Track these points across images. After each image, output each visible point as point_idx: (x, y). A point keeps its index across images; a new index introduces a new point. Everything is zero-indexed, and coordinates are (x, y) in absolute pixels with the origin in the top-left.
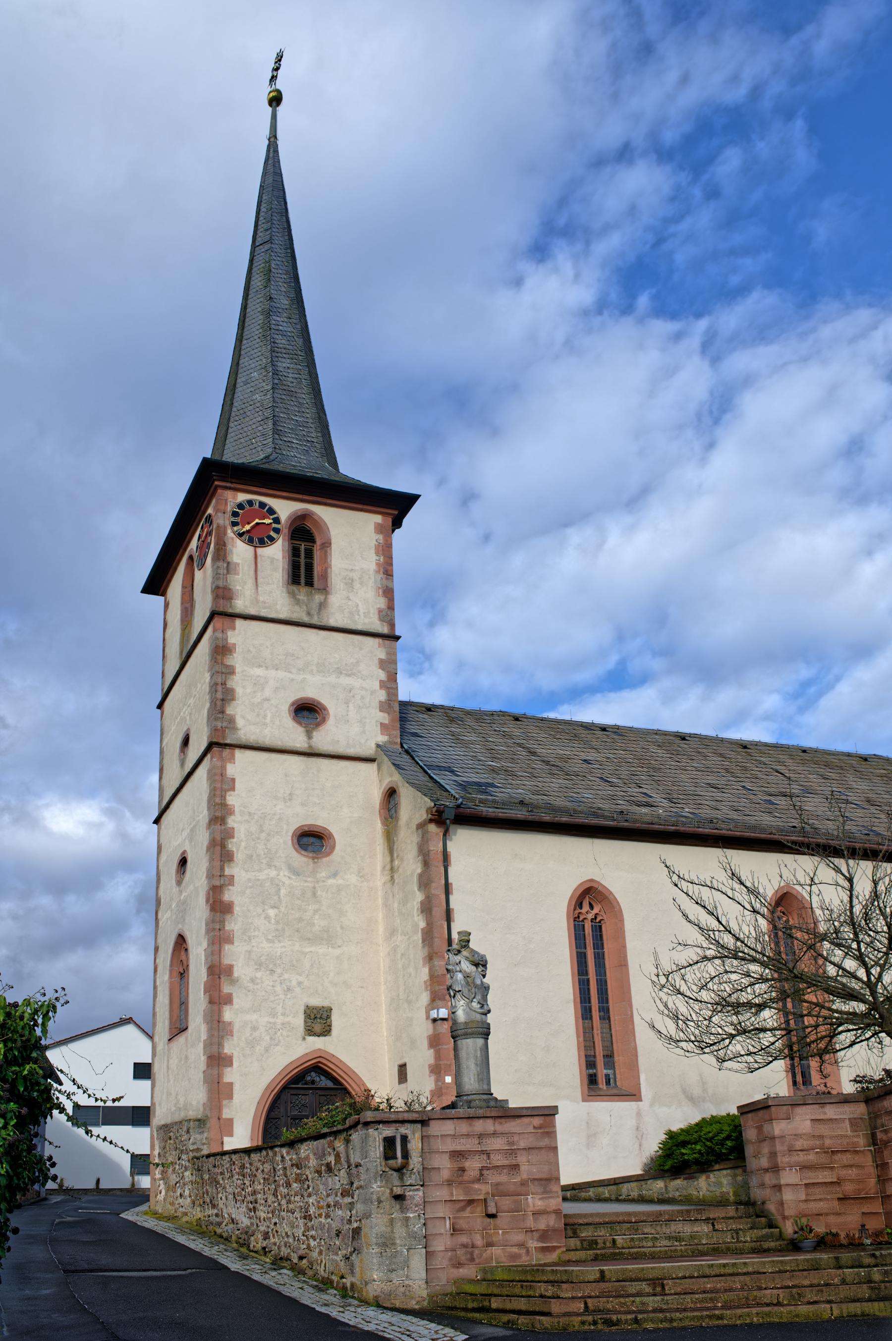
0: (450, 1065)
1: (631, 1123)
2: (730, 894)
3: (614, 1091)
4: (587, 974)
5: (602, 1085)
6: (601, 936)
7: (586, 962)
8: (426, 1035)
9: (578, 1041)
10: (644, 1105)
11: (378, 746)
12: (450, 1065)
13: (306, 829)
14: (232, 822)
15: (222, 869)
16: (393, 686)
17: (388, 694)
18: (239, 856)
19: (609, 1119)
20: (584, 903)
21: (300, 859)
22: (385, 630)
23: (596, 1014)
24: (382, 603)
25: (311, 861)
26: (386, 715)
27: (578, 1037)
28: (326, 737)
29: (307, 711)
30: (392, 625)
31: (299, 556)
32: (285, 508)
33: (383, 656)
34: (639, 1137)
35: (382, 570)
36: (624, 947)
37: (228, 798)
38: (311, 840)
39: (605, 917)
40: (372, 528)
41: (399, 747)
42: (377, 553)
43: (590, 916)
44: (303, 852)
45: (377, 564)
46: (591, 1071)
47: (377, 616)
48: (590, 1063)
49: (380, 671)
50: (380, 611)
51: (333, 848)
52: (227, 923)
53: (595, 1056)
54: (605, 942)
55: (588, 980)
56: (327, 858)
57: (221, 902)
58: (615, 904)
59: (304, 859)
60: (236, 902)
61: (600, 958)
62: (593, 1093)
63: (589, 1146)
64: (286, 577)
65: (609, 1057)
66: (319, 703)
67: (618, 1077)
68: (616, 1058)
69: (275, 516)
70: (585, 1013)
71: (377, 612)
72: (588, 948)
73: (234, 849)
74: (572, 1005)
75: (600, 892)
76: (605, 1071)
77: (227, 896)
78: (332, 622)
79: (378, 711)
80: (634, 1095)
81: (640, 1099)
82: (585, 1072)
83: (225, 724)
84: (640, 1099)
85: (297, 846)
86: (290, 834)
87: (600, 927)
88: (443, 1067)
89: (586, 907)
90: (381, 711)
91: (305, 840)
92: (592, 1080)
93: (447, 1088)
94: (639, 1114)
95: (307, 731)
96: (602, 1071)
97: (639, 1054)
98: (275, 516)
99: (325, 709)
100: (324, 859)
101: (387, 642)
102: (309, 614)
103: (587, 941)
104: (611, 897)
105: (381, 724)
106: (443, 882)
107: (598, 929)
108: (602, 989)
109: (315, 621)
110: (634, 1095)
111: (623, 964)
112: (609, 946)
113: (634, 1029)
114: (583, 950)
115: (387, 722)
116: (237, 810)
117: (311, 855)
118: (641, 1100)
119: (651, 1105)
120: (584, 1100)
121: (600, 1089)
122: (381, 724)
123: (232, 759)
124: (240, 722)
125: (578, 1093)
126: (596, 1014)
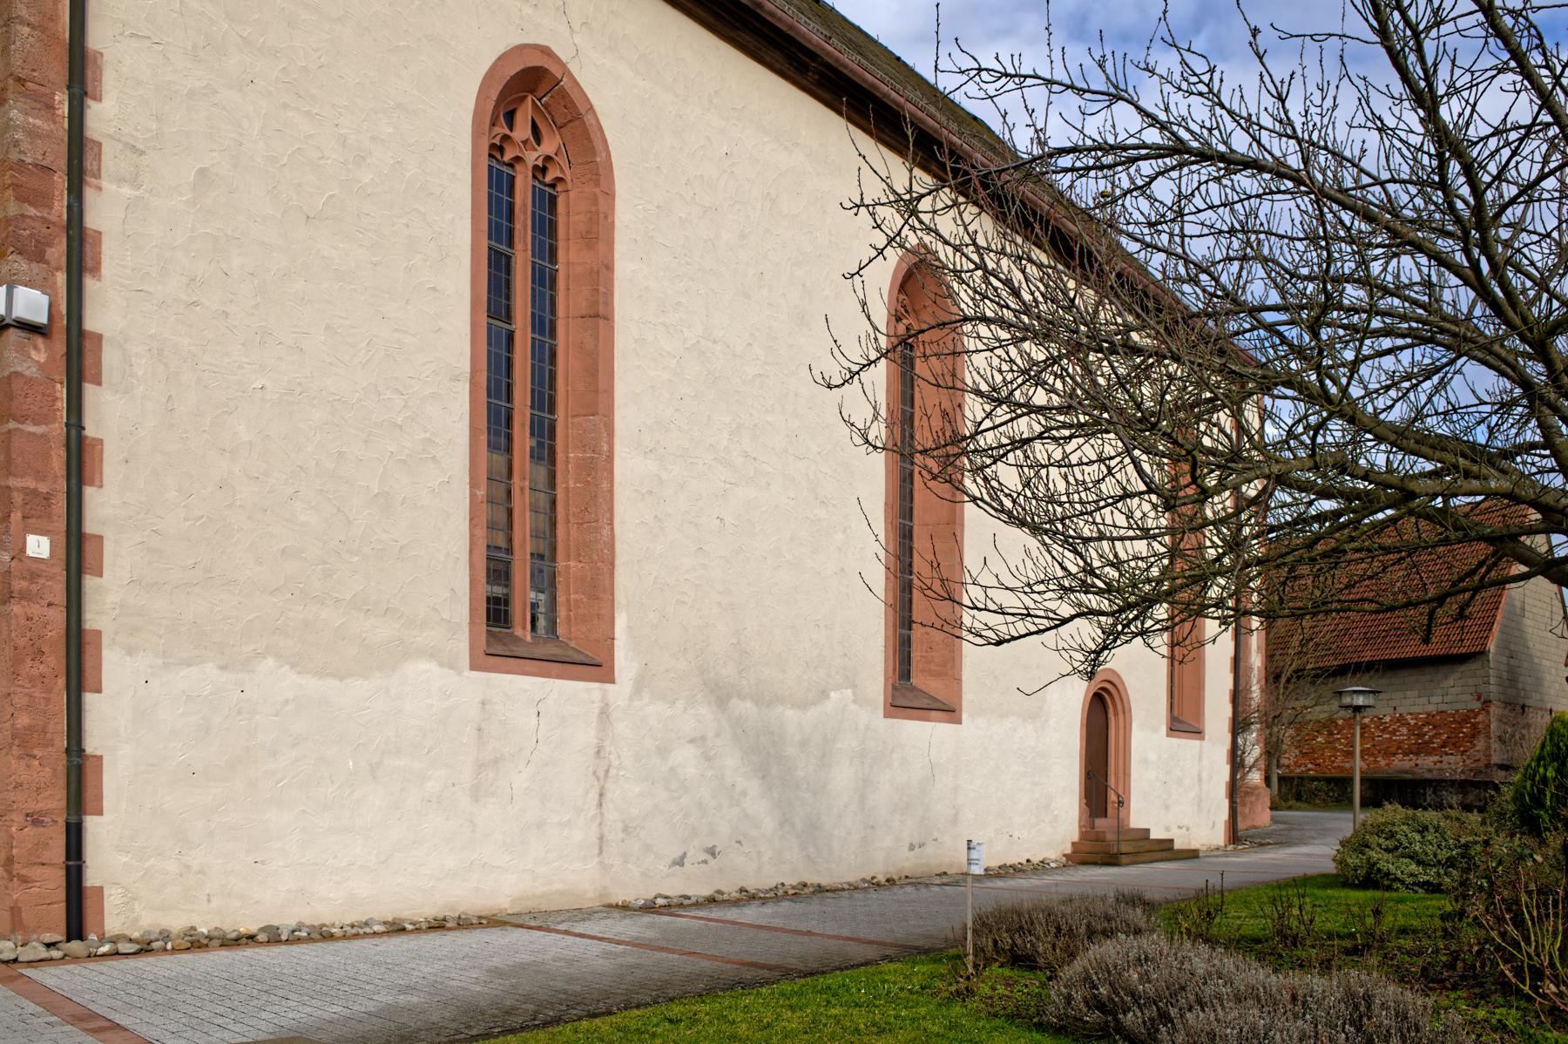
0: (47, 498)
1: (586, 736)
2: (533, 923)
3: (551, 650)
4: (509, 318)
5: (522, 631)
6: (553, 226)
7: (508, 282)
8: (107, 817)
9: (473, 496)
10: (620, 690)
12: (47, 498)
19: (533, 720)
20: (519, 117)
23: (523, 440)
27: (473, 485)
34: (601, 773)
36: (610, 268)
39: (568, 176)
43: (532, 157)
46: (498, 591)
48: (497, 568)
53: (510, 550)
54: (561, 245)
55: (510, 337)
58: (598, 143)
61: (545, 281)
62: (499, 650)
63: (477, 794)
65: (545, 558)
67: (562, 612)
68: (561, 564)
70: (495, 424)
72: (519, 245)
74: (464, 390)
75: (564, 94)
76: (533, 595)
80: (593, 664)
81: (609, 678)
82: (484, 589)
84: (609, 678)
87: (553, 200)
88: (18, 498)
89: (522, 132)
92: (497, 613)
93: (34, 576)
94: (604, 714)
96: (524, 594)
97: (618, 562)
103: (518, 226)
104: (588, 118)
105: (99, 384)
107: (547, 202)
108: (541, 394)
110: (593, 664)
111: (599, 315)
112: (569, 256)
113: (611, 491)
114: (503, 248)
118: (613, 682)
119: (637, 691)
120: (474, 666)
121: (518, 640)
125: (460, 645)
126: (523, 440)
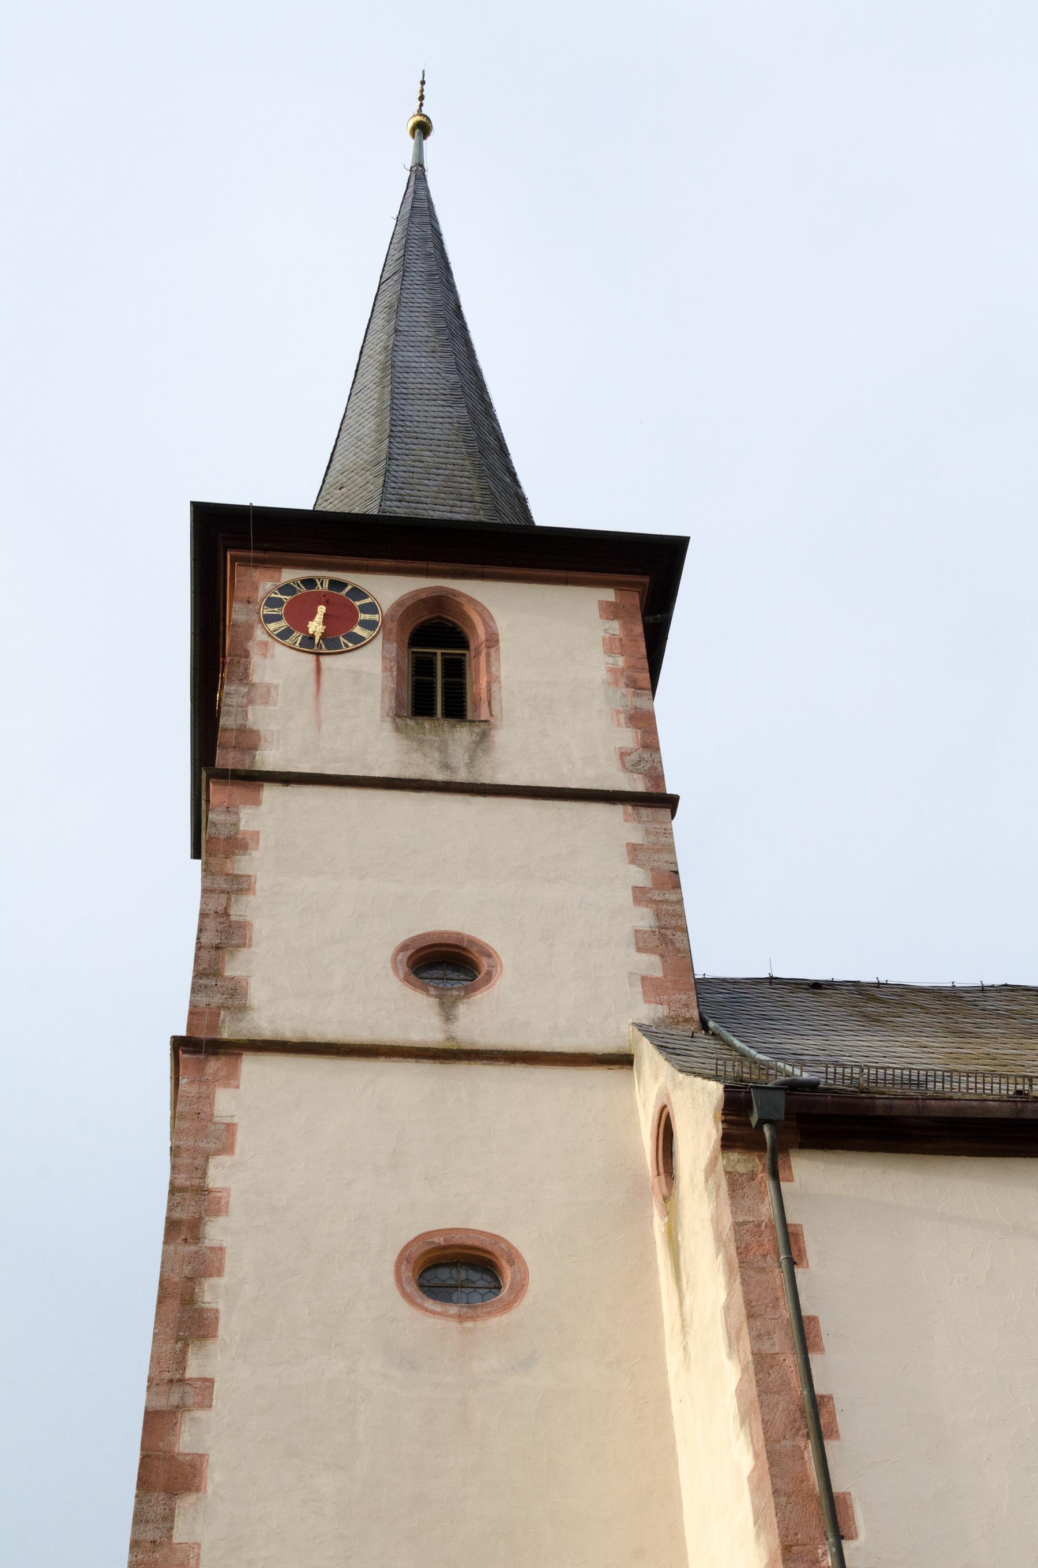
11: (640, 1027)
13: (441, 1240)
14: (216, 1232)
15: (181, 1362)
16: (671, 896)
17: (658, 916)
18: (230, 1326)
21: (430, 1325)
22: (639, 785)
24: (628, 738)
25: (453, 1325)
26: (655, 959)
28: (482, 1018)
29: (444, 963)
30: (657, 777)
31: (446, 686)
32: (388, 590)
33: (637, 837)
35: (622, 681)
37: (212, 1171)
38: (458, 1271)
40: (594, 610)
41: (694, 1027)
42: (609, 651)
44: (430, 1304)
45: (612, 671)
47: (616, 763)
49: (634, 868)
50: (623, 754)
51: (520, 1288)
52: (179, 1523)
56: (504, 1318)
57: (171, 1458)
59: (431, 1321)
60: (212, 1459)
64: (390, 702)
66: (473, 942)
69: (349, 588)
71: (616, 757)
73: (221, 1306)
77: (187, 1440)
78: (503, 778)
79: (632, 950)
83: (217, 1000)
85: (412, 1289)
86: (392, 1256)
90: (639, 950)
91: (444, 1275)
95: (442, 1004)
98: (349, 588)
99: (488, 954)
100: (494, 1321)
101: (645, 812)
102: (446, 766)
105: (644, 979)
106: (786, 1312)
109: (462, 776)
115: (659, 973)
116: (235, 1201)
117: (453, 1309)
122: (644, 979)
123: (231, 1078)
124: (257, 994)
